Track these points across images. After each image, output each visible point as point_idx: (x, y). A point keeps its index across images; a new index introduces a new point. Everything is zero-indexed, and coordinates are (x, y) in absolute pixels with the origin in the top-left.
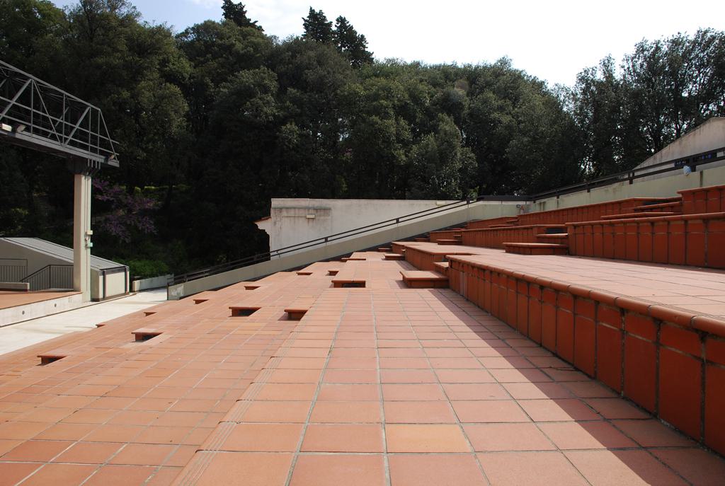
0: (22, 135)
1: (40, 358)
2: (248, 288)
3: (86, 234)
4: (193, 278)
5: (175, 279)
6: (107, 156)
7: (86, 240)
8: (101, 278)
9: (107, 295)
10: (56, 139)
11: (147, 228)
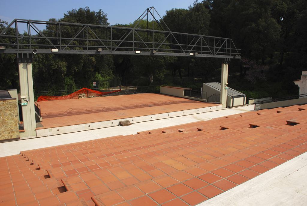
0: (198, 55)
1: (287, 122)
2: (121, 124)
3: (225, 85)
4: (266, 101)
5: (272, 100)
6: (235, 55)
7: (225, 87)
8: (232, 100)
9: (234, 106)
10: (211, 54)
11: (263, 78)
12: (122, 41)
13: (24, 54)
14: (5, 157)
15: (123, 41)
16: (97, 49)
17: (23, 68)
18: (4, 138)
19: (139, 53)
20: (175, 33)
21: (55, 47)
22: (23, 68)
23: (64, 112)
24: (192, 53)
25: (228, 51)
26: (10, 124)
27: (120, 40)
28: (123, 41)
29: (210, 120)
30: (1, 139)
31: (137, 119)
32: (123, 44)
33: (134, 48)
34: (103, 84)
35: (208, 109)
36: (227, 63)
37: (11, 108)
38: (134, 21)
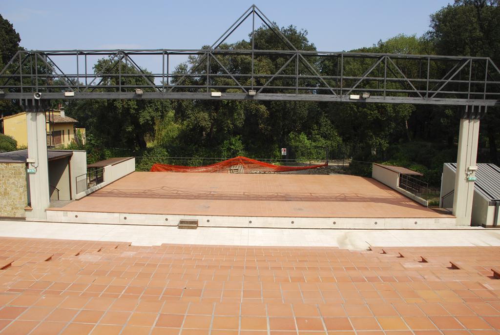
12: (448, 81)
13: (28, 100)
15: (449, 80)
16: (133, 89)
17: (31, 119)
18: (5, 215)
19: (72, 96)
20: (443, 57)
22: (31, 119)
23: (338, 195)
24: (354, 93)
25: (480, 88)
26: (13, 197)
27: (444, 79)
28: (449, 80)
29: (471, 245)
30: (2, 216)
32: (450, 87)
34: (311, 153)
36: (475, 118)
37: (14, 174)
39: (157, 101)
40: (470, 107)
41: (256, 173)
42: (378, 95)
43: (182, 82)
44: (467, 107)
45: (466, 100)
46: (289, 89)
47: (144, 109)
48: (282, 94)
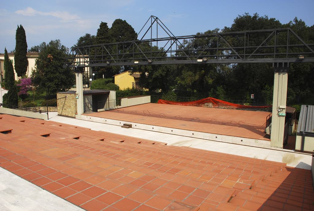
13: (279, 63)
14: (63, 123)
16: (296, 56)
21: (240, 57)
31: (139, 125)
33: (245, 54)
35: (252, 142)
38: (206, 30)
39: (164, 66)
40: (276, 64)
41: (221, 108)
42: (259, 58)
43: (183, 53)
44: (273, 64)
45: (273, 59)
46: (271, 55)
47: (157, 70)
48: (164, 61)
